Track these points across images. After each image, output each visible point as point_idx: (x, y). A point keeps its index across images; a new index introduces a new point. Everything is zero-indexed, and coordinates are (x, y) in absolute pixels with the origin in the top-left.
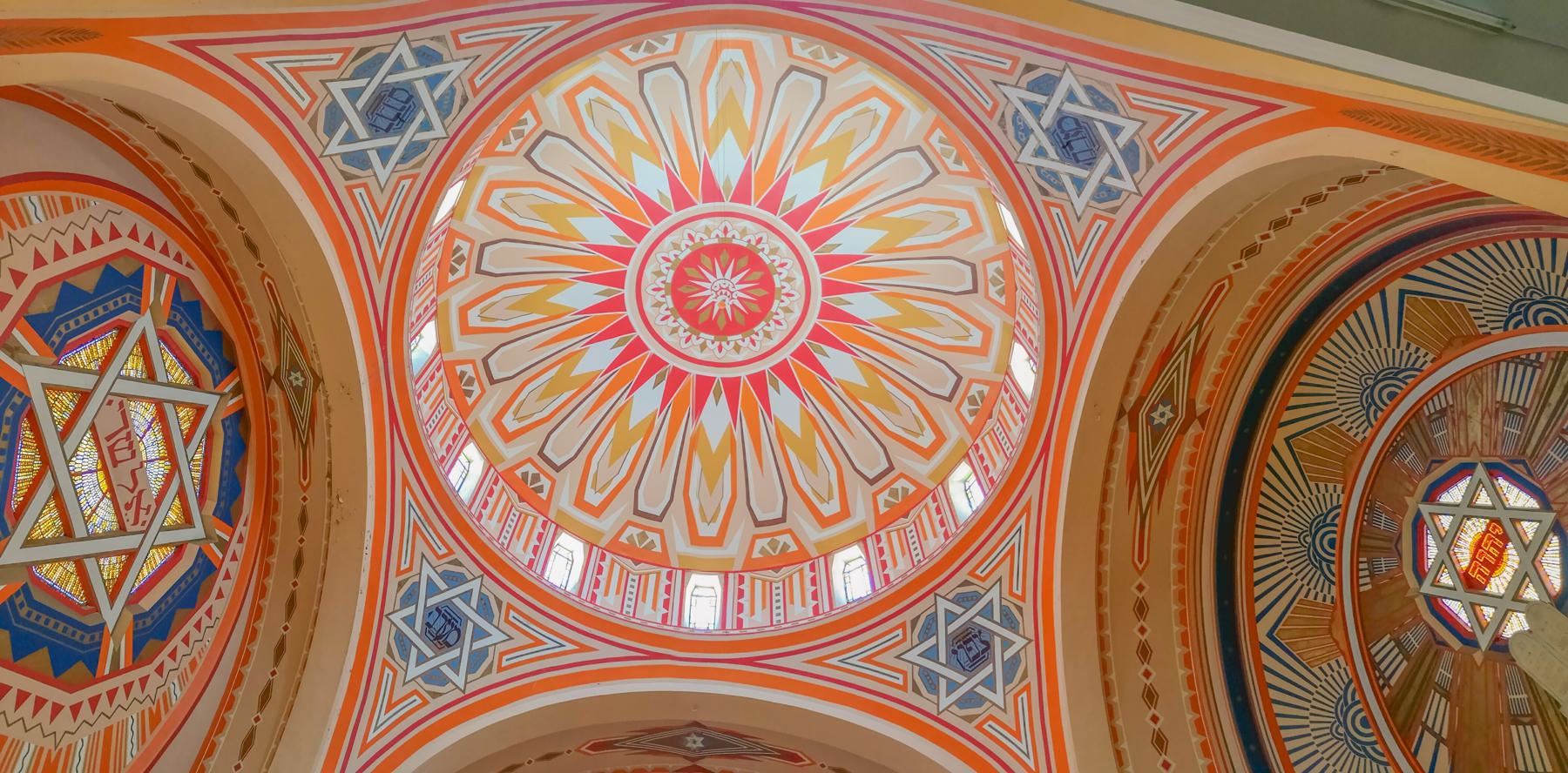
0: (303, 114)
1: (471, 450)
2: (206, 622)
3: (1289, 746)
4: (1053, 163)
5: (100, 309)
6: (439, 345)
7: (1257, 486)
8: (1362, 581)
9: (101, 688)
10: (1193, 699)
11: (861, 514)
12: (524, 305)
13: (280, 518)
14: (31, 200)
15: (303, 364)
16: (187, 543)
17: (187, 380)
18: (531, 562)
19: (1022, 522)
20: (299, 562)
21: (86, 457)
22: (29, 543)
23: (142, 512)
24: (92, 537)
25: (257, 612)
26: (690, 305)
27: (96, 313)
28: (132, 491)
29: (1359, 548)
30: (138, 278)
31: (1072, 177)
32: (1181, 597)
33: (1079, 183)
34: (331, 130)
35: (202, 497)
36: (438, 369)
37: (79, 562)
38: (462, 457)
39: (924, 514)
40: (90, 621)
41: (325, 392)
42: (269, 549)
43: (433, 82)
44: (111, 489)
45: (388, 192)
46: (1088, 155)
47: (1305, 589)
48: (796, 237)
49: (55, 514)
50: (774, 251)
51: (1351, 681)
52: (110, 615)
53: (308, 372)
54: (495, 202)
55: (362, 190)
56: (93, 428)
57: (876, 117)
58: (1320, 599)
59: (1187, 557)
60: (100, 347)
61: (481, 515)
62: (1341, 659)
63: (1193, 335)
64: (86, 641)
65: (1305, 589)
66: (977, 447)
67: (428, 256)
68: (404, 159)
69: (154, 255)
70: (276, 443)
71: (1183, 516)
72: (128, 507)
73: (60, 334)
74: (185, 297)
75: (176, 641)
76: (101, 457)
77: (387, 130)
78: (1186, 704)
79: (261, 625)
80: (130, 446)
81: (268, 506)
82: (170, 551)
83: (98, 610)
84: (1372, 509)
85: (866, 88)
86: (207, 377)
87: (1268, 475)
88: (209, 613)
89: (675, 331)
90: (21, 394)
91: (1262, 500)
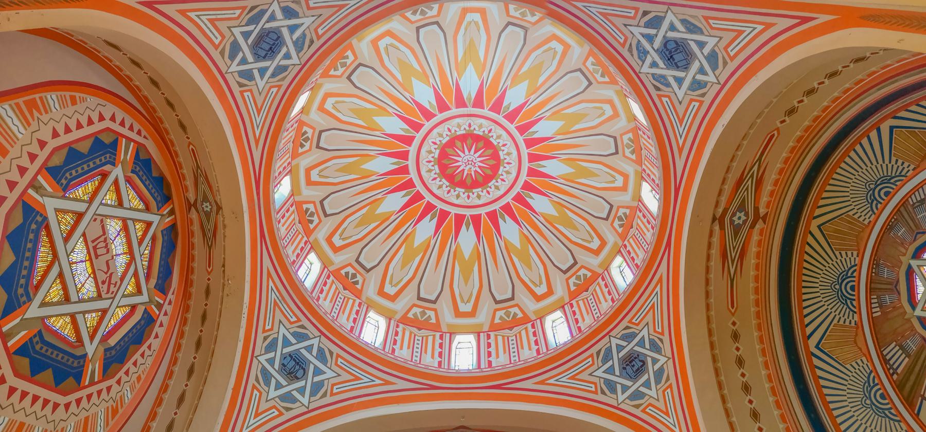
0: (216, 47)
1: (312, 257)
2: (148, 353)
3: (835, 413)
4: (663, 70)
5: (91, 163)
6: (292, 190)
7: (801, 257)
8: (873, 306)
9: (83, 393)
10: (772, 388)
11: (560, 291)
12: (345, 169)
13: (193, 290)
14: (52, 98)
15: (211, 198)
16: (138, 304)
17: (141, 206)
18: (352, 328)
19: (658, 289)
20: (204, 317)
21: (80, 252)
22: (43, 304)
23: (112, 286)
24: (81, 301)
25: (178, 347)
26: (449, 171)
27: (89, 166)
28: (106, 273)
29: (870, 291)
30: (115, 145)
31: (674, 77)
32: (759, 328)
33: (680, 81)
34: (232, 57)
35: (148, 277)
36: (292, 206)
37: (73, 316)
38: (306, 261)
39: (598, 289)
40: (78, 352)
41: (223, 216)
42: (187, 309)
43: (292, 29)
44: (94, 272)
45: (264, 95)
46: (684, 62)
47: (838, 317)
48: (512, 128)
49: (60, 287)
50: (499, 137)
51: (871, 372)
52: (90, 348)
53: (213, 204)
54: (328, 106)
55: (249, 93)
56: (84, 235)
57: (555, 53)
58: (847, 323)
59: (761, 303)
60: (90, 186)
61: (319, 298)
62: (864, 359)
63: (756, 168)
64: (75, 365)
65: (838, 317)
66: (625, 246)
67: (287, 137)
68: (273, 75)
69: (125, 131)
70: (193, 244)
71: (757, 278)
72: (103, 283)
73: (66, 178)
74: (142, 156)
75: (129, 364)
76: (89, 252)
77: (264, 57)
78: (773, 405)
79: (180, 355)
80: (106, 246)
81: (187, 282)
82: (127, 310)
83: (83, 345)
84: (878, 265)
85: (549, 35)
86: (153, 204)
87: (807, 249)
88: (149, 347)
89: (440, 187)
90: (41, 215)
91: (806, 265)
